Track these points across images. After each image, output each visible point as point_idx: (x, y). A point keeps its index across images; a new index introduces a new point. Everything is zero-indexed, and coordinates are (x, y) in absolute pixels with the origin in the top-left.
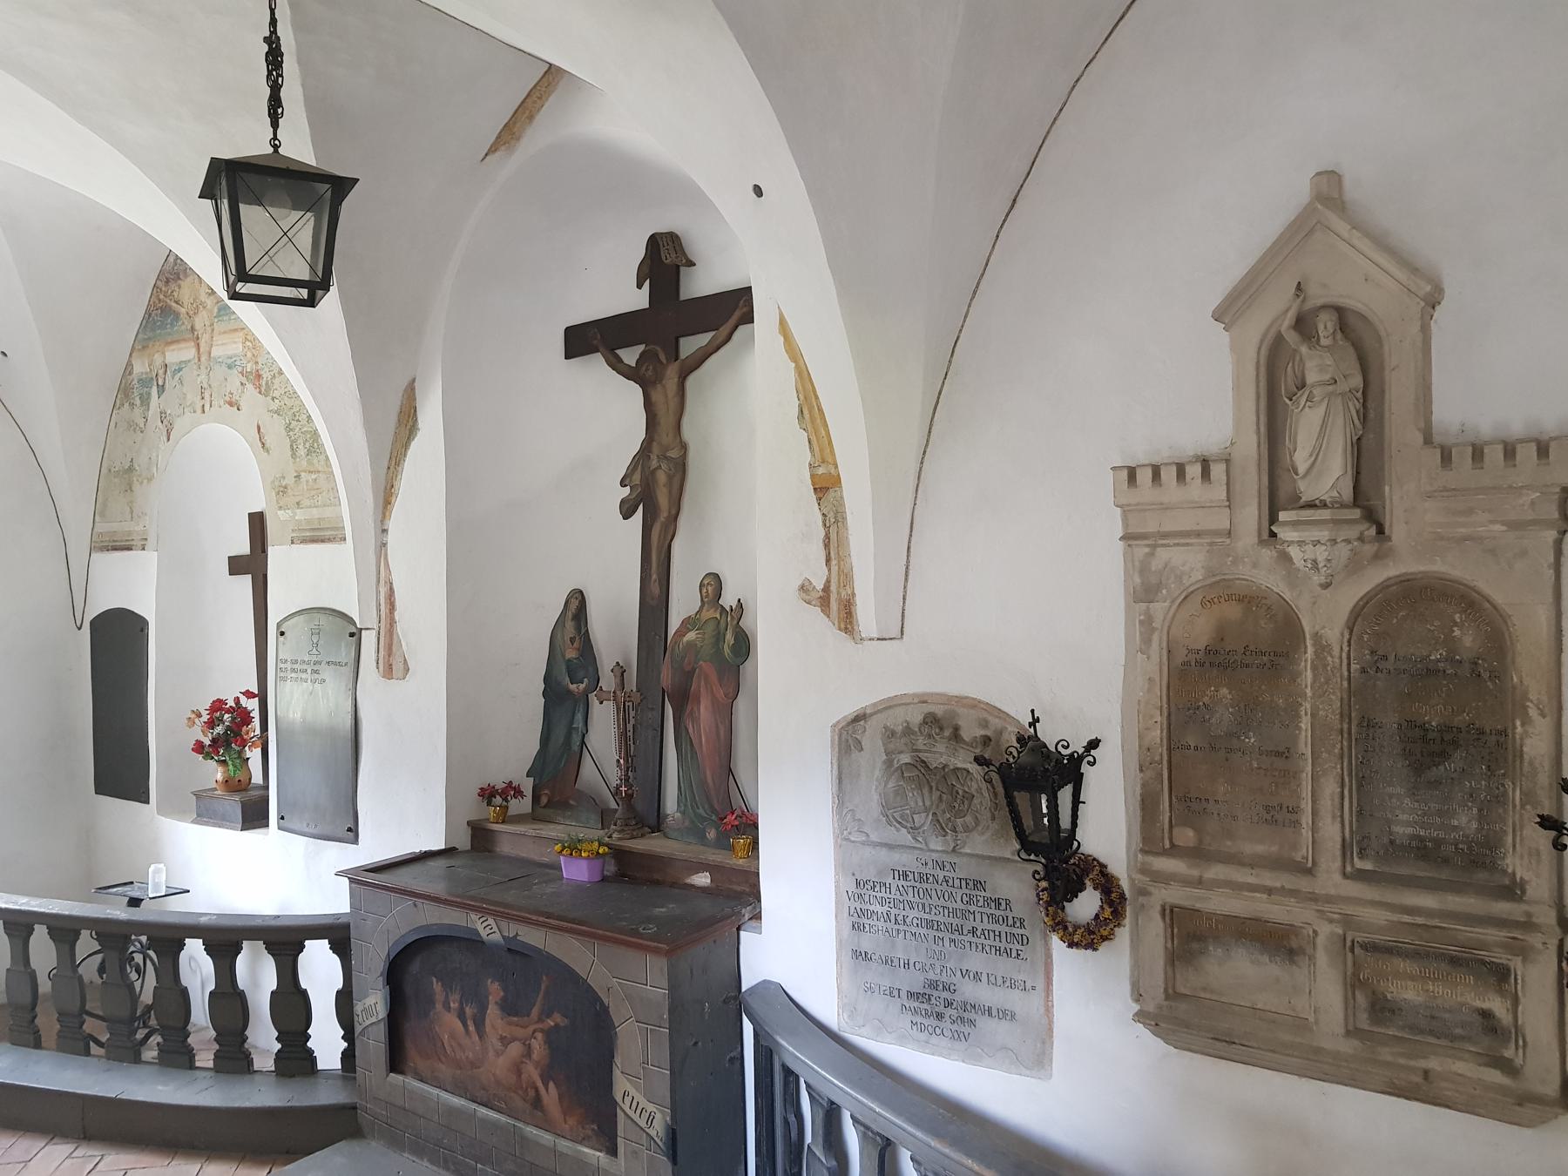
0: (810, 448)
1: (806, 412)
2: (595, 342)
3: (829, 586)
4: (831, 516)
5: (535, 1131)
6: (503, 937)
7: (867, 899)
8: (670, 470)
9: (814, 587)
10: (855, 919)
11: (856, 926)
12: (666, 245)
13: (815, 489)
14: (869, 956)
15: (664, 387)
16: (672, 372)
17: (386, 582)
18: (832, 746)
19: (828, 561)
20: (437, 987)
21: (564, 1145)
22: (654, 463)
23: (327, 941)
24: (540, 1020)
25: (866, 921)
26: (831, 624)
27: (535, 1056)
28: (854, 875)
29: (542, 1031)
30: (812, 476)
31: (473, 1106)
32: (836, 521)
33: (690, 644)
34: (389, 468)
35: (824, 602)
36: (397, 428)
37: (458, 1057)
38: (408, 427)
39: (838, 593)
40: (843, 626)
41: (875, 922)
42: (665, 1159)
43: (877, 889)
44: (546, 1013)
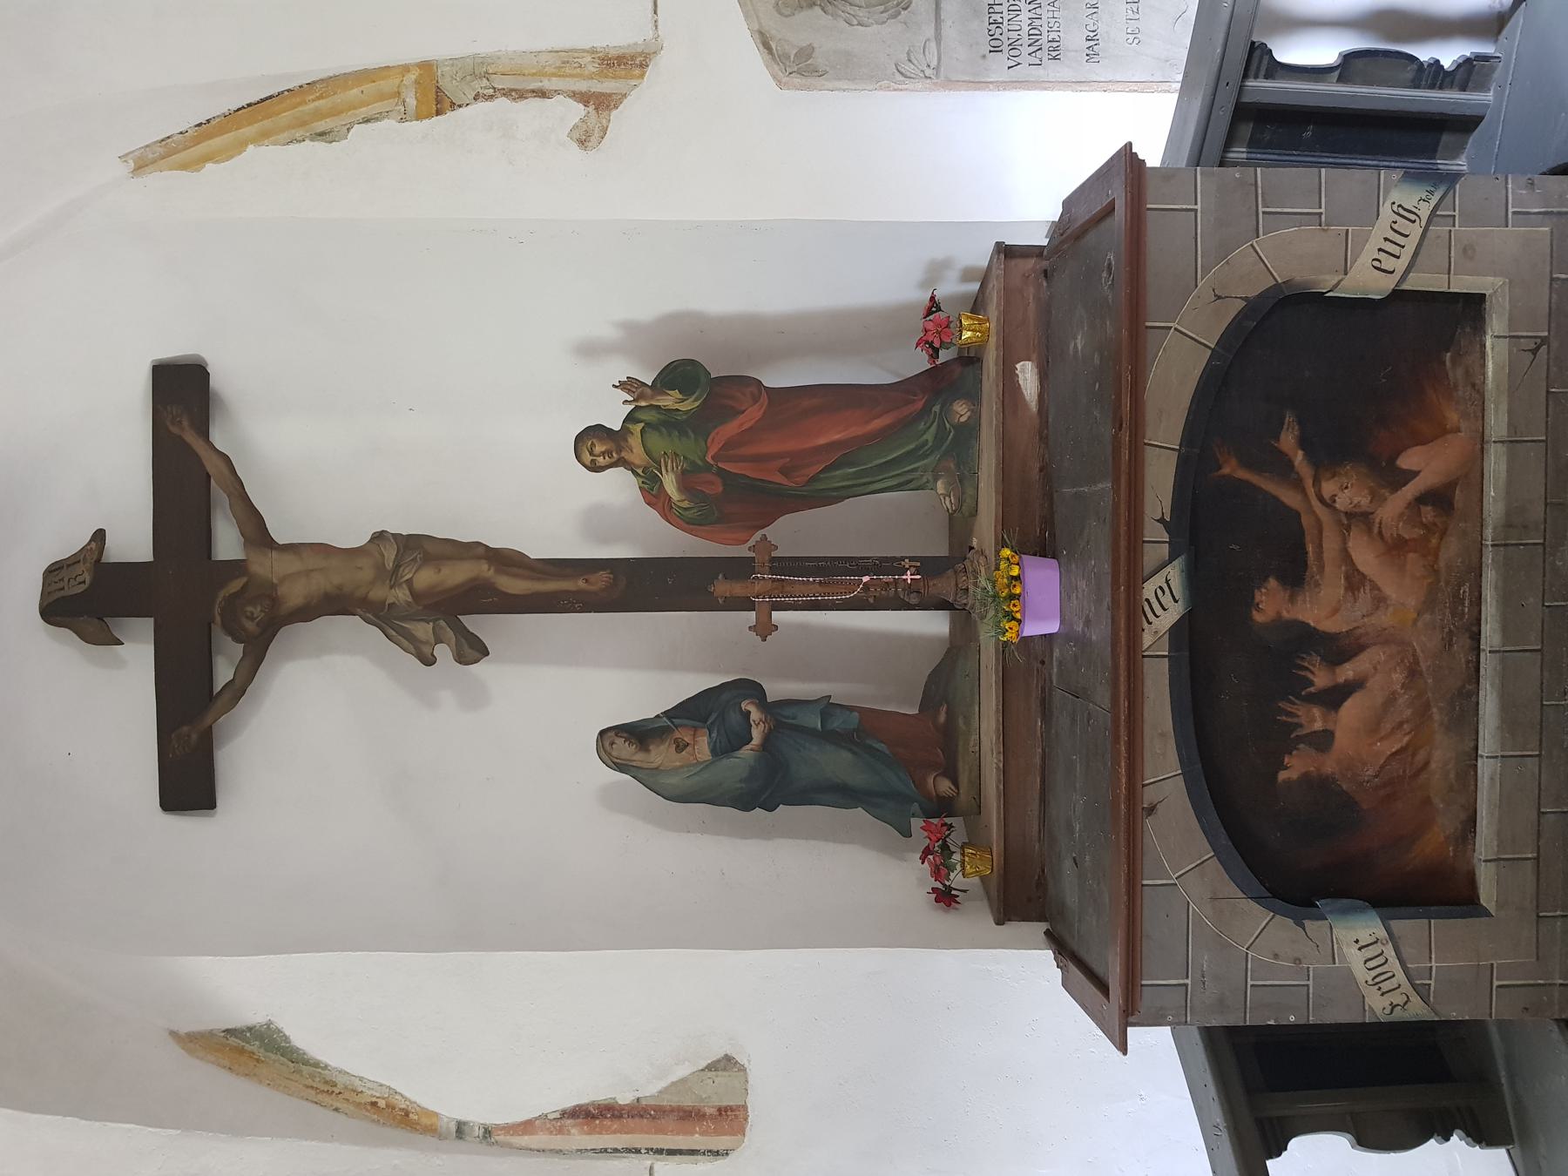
0: (377, 119)
1: (321, 126)
2: (194, 737)
3: (581, 93)
4: (480, 85)
5: (1491, 492)
6: (1172, 557)
7: (1014, 35)
8: (414, 560)
9: (581, 120)
10: (1044, 54)
11: (1054, 54)
12: (60, 585)
13: (438, 113)
14: (1092, 34)
15: (283, 579)
16: (266, 567)
17: (560, 1131)
18: (808, 88)
19: (542, 94)
20: (1294, 768)
21: (1497, 422)
22: (401, 595)
23: (1269, 1163)
24: (1298, 485)
25: (1044, 39)
26: (637, 90)
27: (1363, 501)
28: (984, 56)
29: (1317, 481)
30: (419, 118)
31: (1488, 664)
32: (487, 75)
33: (684, 485)
34: (336, 1110)
35: (602, 103)
36: (260, 1082)
37: (1409, 712)
38: (261, 1053)
39: (591, 77)
40: (637, 72)
41: (1044, 21)
42: (1458, 186)
43: (997, 17)
44: (1282, 468)
